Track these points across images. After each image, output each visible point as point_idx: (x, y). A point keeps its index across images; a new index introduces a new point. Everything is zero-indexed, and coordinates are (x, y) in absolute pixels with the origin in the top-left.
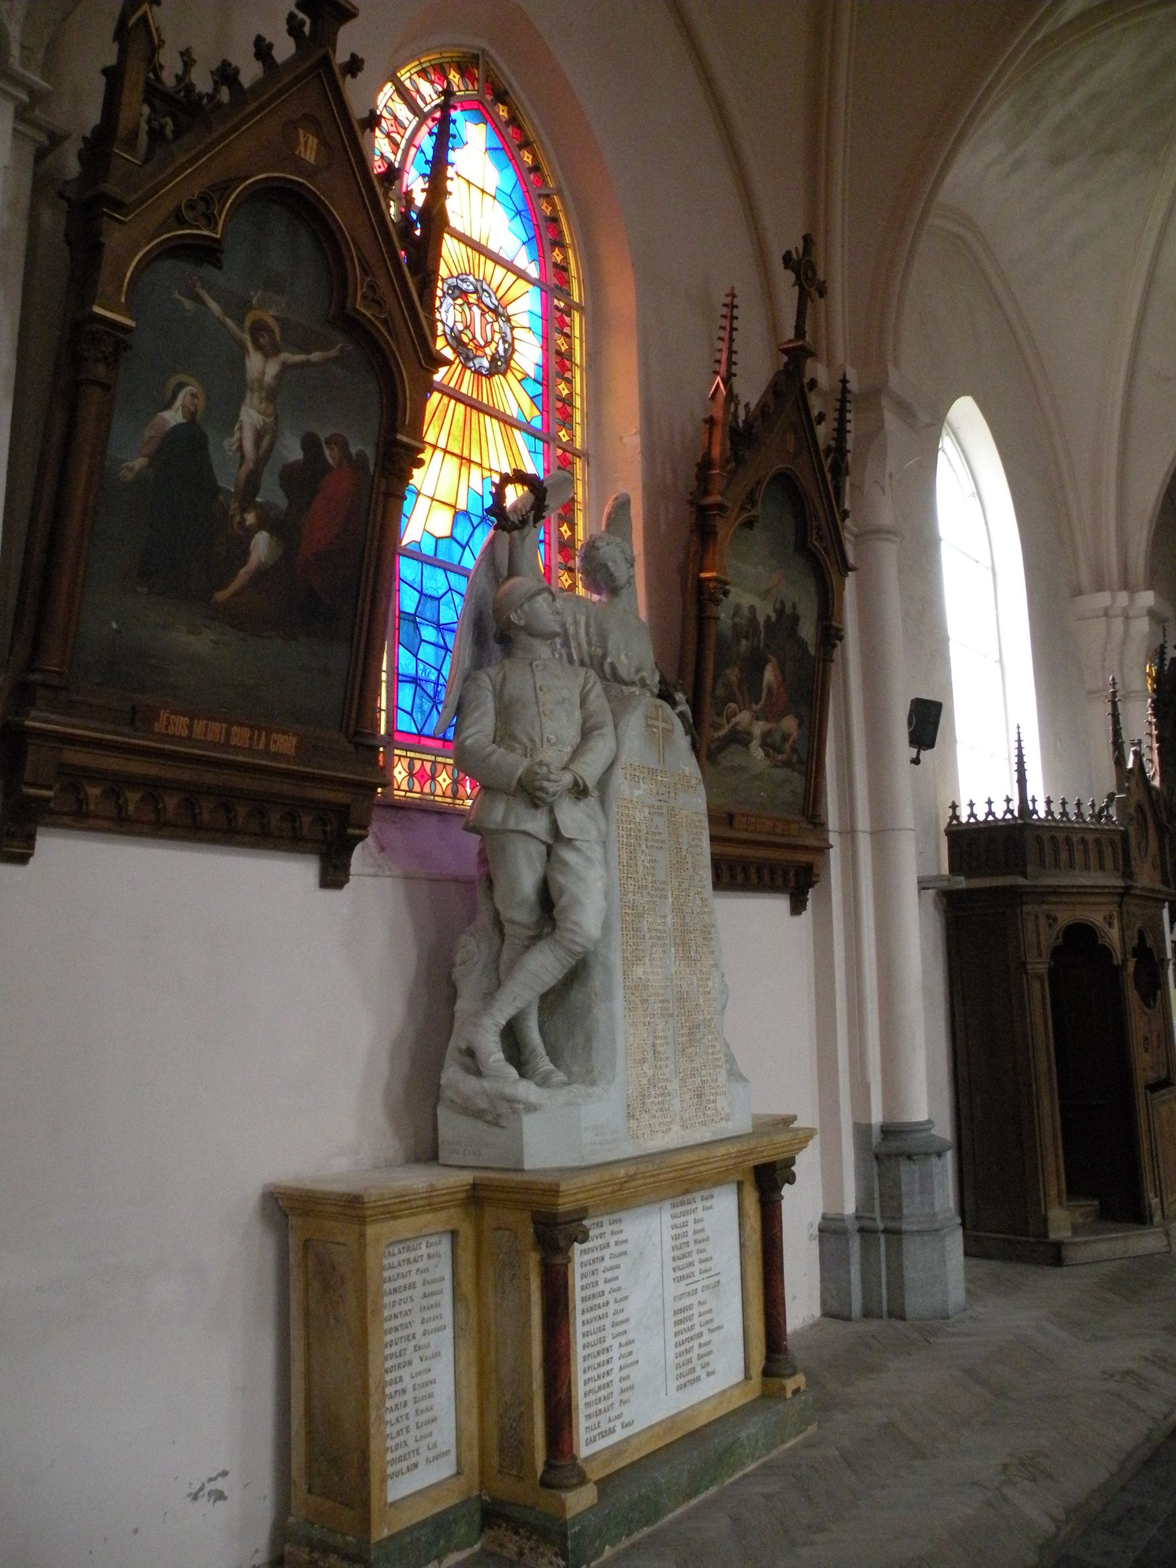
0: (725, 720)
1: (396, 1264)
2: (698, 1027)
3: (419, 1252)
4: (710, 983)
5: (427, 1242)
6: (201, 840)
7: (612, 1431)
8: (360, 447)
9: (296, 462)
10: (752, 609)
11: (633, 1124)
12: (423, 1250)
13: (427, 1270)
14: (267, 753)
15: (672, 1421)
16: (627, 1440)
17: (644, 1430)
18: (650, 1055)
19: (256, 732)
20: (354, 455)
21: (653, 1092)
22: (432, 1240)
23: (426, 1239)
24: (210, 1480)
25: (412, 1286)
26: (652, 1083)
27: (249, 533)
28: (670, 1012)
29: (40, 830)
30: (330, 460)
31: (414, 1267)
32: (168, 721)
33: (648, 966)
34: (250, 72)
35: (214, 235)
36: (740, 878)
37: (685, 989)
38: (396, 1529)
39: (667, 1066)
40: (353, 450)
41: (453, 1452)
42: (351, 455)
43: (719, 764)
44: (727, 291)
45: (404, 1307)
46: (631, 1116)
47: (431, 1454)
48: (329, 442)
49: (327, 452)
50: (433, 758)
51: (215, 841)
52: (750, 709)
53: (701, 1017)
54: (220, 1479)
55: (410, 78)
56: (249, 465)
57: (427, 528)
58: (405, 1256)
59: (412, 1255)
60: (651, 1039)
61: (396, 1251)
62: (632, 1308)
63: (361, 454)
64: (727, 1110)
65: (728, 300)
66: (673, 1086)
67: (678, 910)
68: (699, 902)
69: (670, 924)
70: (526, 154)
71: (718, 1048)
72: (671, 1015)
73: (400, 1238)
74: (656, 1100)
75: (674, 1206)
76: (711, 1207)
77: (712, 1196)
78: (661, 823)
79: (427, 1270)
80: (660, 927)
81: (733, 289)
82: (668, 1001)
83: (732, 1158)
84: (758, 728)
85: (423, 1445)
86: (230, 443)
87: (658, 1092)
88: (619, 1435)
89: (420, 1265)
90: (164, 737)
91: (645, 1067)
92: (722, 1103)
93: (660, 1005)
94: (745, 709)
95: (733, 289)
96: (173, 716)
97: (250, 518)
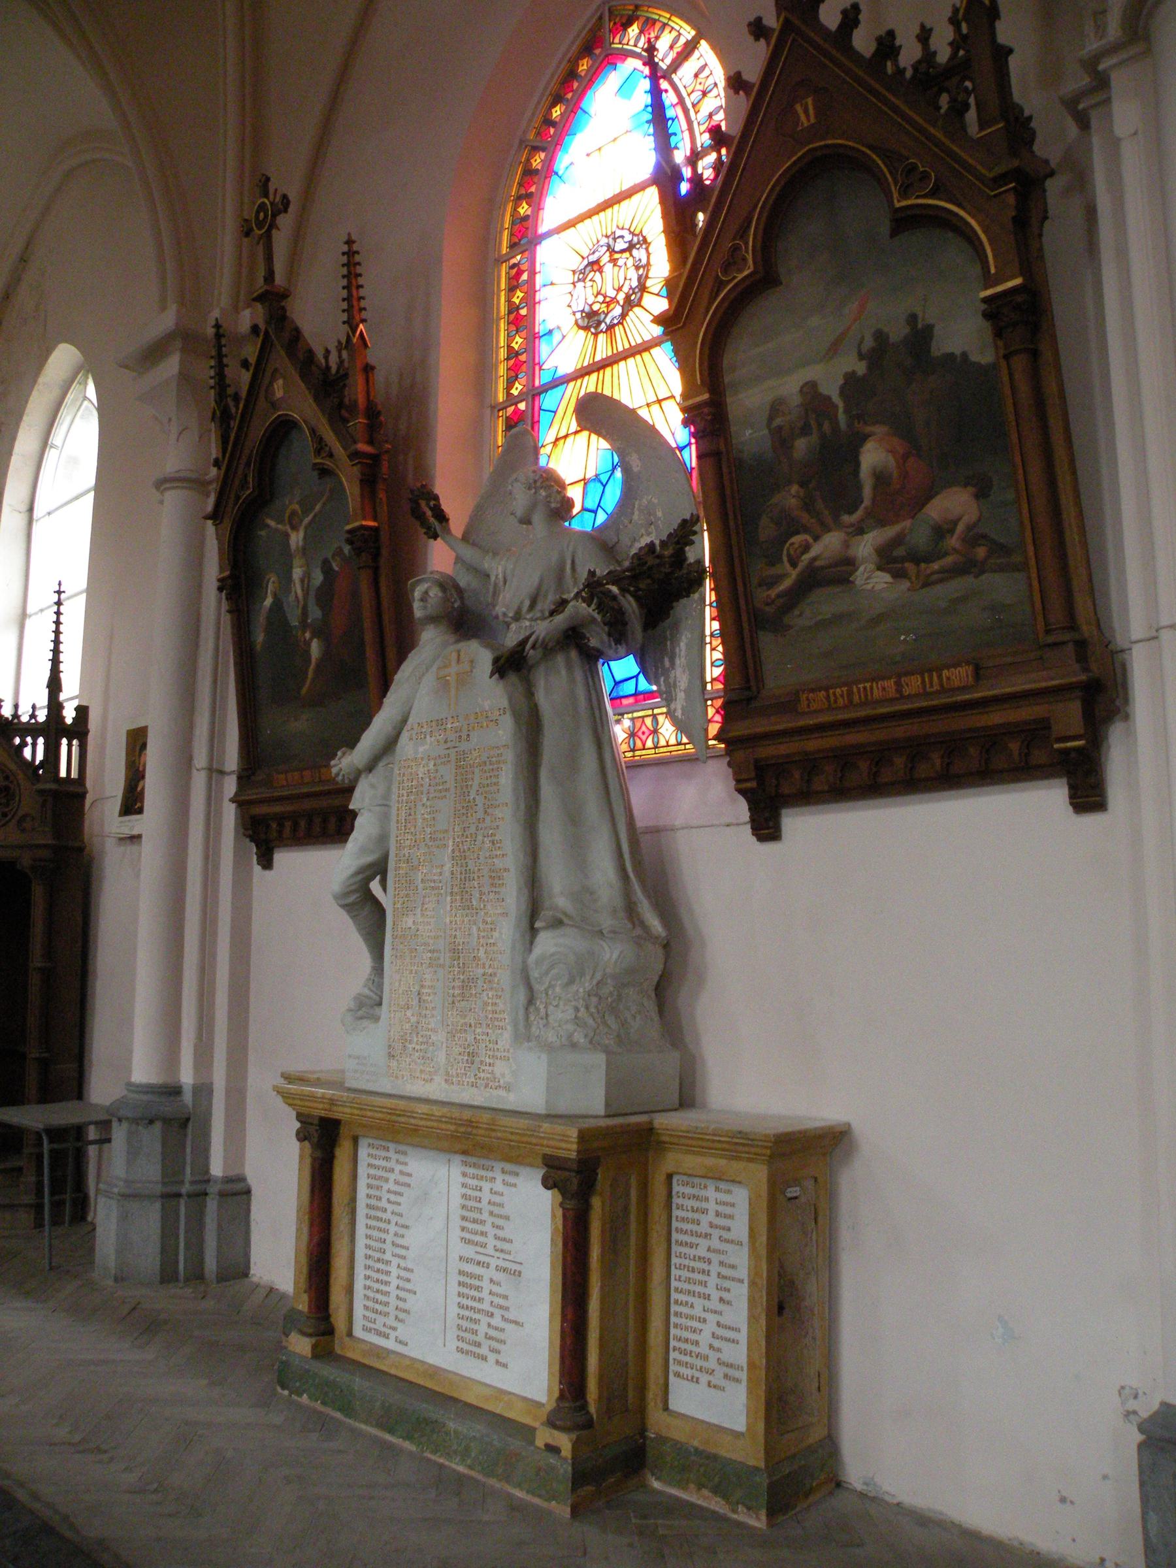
0: (787, 565)
2: (474, 980)
4: (496, 934)
6: (993, 783)
7: (387, 1336)
10: (810, 390)
11: (394, 1064)
14: (943, 690)
15: (435, 1372)
16: (389, 1352)
18: (415, 1002)
19: (926, 675)
21: (415, 1039)
26: (415, 1028)
27: (308, 644)
28: (441, 961)
29: (276, 850)
32: (808, 699)
33: (419, 916)
34: (863, 41)
35: (895, 201)
36: (317, 829)
37: (459, 940)
39: (433, 1016)
43: (790, 627)
44: (345, 238)
46: (391, 1056)
50: (650, 712)
51: (898, 793)
52: (839, 525)
53: (480, 971)
55: (662, 60)
56: (302, 602)
57: (593, 515)
60: (417, 987)
62: (414, 1238)
64: (508, 1078)
65: (345, 248)
66: (440, 1037)
67: (460, 856)
68: (488, 845)
69: (447, 874)
70: (555, 115)
71: (501, 1006)
72: (442, 966)
74: (418, 1047)
75: (465, 1163)
76: (515, 1185)
77: (517, 1174)
78: (448, 773)
80: (436, 878)
81: (349, 234)
82: (438, 951)
83: (324, 1103)
84: (866, 547)
86: (292, 598)
87: (420, 1040)
88: (389, 1344)
91: (409, 1013)
92: (500, 1068)
93: (429, 955)
95: (349, 234)
96: (811, 695)
97: (308, 635)
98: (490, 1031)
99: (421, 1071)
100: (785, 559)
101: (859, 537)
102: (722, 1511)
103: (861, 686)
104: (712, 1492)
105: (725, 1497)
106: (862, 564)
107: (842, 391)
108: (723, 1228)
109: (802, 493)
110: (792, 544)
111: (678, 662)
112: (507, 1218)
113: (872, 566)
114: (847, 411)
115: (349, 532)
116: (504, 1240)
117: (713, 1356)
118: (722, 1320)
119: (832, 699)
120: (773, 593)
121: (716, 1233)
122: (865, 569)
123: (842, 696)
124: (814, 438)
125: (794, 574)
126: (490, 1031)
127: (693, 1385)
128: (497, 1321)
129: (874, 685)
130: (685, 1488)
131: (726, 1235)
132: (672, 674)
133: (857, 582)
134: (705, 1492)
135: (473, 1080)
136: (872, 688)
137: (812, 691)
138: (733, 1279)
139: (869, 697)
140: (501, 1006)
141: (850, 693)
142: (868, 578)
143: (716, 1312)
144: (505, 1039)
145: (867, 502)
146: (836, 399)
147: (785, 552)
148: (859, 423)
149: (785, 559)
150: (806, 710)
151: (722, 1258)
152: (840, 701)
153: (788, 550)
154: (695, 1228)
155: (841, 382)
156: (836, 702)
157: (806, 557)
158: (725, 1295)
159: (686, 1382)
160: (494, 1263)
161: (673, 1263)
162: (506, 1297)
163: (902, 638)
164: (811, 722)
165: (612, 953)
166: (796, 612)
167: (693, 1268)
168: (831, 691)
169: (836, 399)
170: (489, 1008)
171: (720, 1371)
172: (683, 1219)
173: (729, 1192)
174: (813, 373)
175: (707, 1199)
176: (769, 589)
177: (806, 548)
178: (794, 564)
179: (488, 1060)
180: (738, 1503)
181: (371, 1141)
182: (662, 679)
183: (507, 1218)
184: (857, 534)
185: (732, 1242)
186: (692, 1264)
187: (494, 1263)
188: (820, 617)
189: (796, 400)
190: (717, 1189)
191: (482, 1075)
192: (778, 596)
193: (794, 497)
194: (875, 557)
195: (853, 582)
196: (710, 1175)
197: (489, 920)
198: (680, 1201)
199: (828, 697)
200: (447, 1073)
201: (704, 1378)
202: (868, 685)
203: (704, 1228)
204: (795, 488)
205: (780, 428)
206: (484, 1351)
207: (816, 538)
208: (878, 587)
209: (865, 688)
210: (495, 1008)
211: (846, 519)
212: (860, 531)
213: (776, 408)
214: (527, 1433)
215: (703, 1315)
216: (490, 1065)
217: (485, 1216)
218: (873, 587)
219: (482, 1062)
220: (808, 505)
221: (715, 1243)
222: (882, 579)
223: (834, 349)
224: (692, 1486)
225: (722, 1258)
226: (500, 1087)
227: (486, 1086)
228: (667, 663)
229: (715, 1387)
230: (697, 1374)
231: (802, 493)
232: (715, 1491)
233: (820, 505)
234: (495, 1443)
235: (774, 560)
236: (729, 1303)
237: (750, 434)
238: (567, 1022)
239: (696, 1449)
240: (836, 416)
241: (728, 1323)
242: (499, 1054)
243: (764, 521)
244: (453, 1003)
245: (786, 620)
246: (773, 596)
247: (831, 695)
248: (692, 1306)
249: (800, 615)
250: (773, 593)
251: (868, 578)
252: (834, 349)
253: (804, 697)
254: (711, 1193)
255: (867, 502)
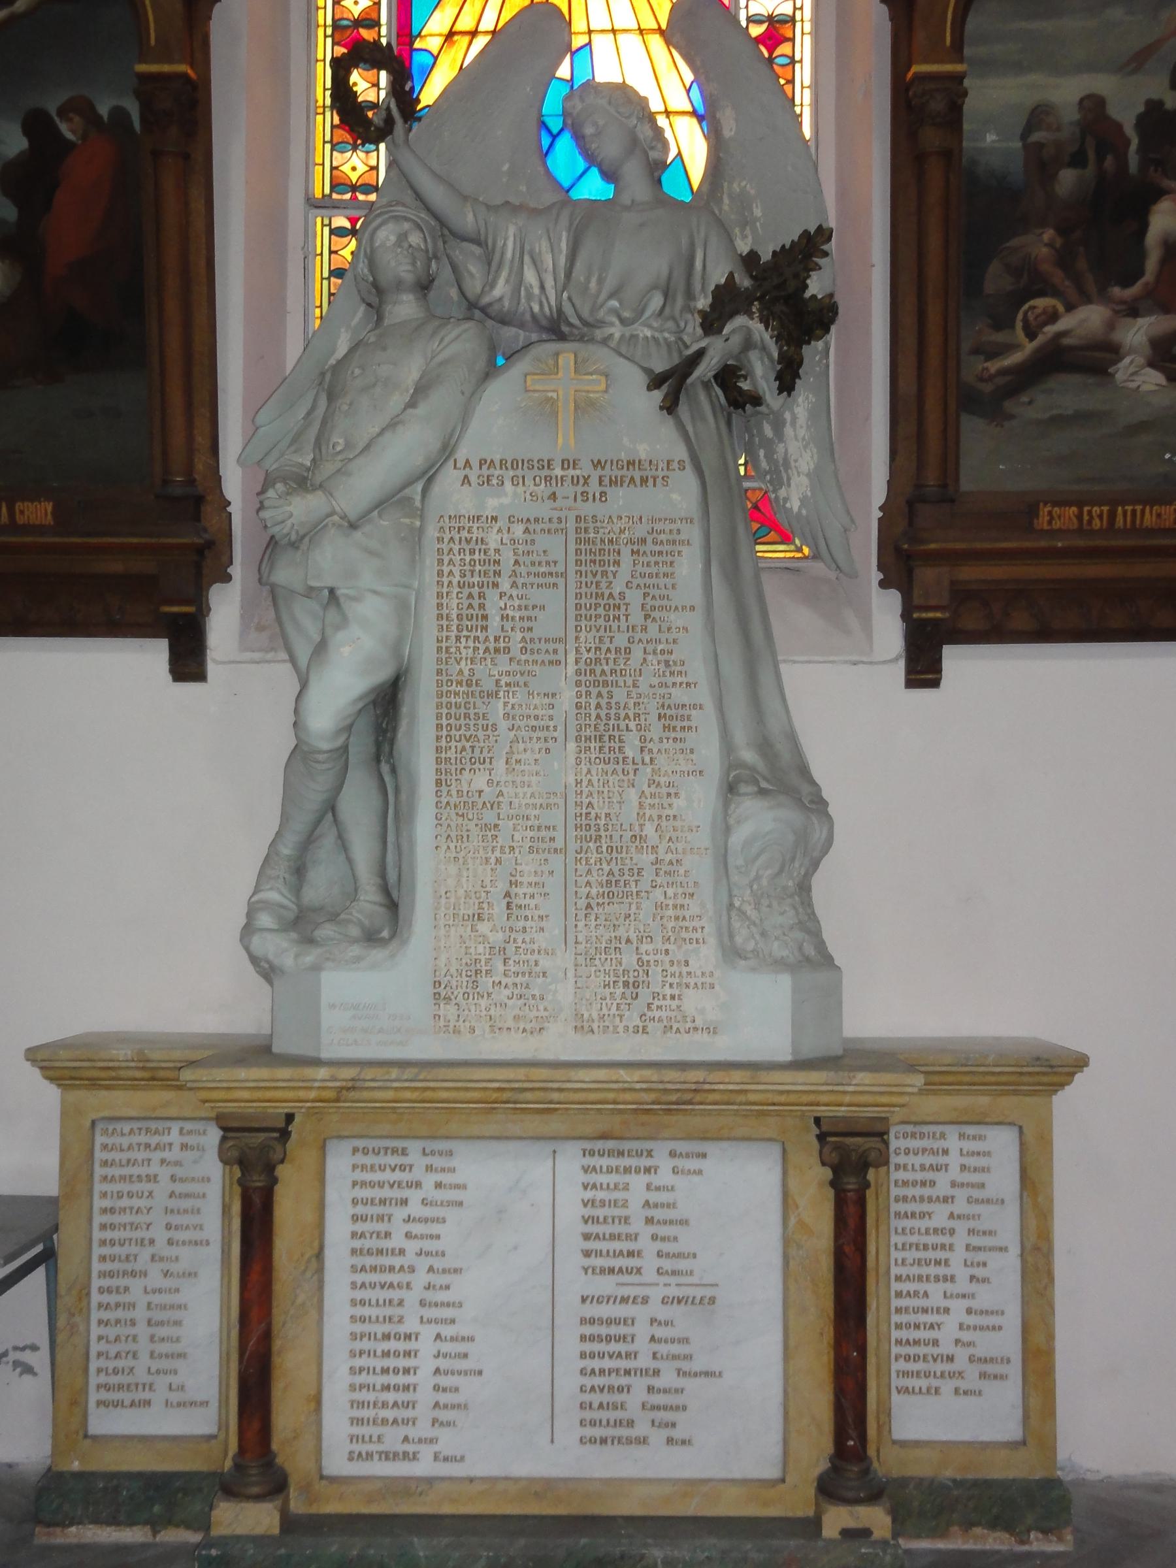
1: (125, 1146)
3: (166, 1139)
4: (679, 803)
5: (181, 1129)
8: (114, 102)
9: (22, 153)
10: (1094, 105)
12: (174, 1137)
13: (178, 1163)
15: (545, 1487)
16: (430, 1481)
17: (165, 1438)
18: (499, 908)
20: (105, 117)
22: (188, 1126)
23: (181, 1124)
24: (16, 1348)
25: (153, 1178)
30: (70, 136)
31: (157, 1156)
32: (1050, 513)
37: (600, 808)
38: (92, 1467)
40: (103, 110)
41: (214, 1404)
42: (101, 117)
45: (136, 1203)
47: (175, 1397)
48: (62, 112)
49: (64, 128)
52: (1103, 296)
54: (28, 1352)
58: (143, 1139)
59: (154, 1140)
61: (126, 1130)
63: (119, 114)
71: (694, 909)
73: (118, 1114)
77: (450, 1153)
79: (178, 1163)
85: (162, 1382)
88: (424, 1467)
89: (166, 1155)
90: (1052, 533)
94: (1088, 301)
96: (1056, 509)
98: (671, 947)
99: (516, 1018)
100: (1019, 325)
101: (1129, 320)
102: (1004, 1548)
103: (1129, 508)
104: (61, 1475)
105: (1009, 1528)
106: (1128, 354)
107: (1142, 122)
108: (972, 1185)
109: (1059, 242)
110: (1033, 308)
111: (788, 431)
112: (684, 1222)
113: (1140, 360)
114: (1141, 149)
115: (144, 78)
116: (679, 1255)
117: (962, 1354)
118: (974, 1304)
119: (1086, 518)
120: (994, 366)
121: (961, 1194)
122: (1132, 362)
123: (1100, 516)
124: (1090, 171)
125: (1030, 347)
126: (671, 947)
127: (932, 1399)
128: (668, 1378)
129: (1148, 508)
130: (943, 1534)
131: (976, 1193)
132: (780, 448)
133: (1117, 376)
134: (978, 1530)
135: (638, 1022)
136: (1143, 512)
137: (1056, 504)
138: (991, 1249)
139: (1138, 522)
140: (694, 909)
141: (1112, 515)
142: (1135, 373)
143: (964, 1296)
144: (706, 956)
145: (1150, 274)
146: (1129, 130)
147: (1020, 316)
148: (1156, 171)
149: (1019, 325)
150: (1046, 527)
151: (972, 1224)
152: (1097, 524)
153: (1026, 313)
154: (927, 1192)
155: (1141, 109)
156: (1090, 522)
157: (1051, 330)
158: (979, 1272)
159: (920, 1397)
160: (656, 1294)
161: (892, 1243)
162: (685, 1341)
163: (1167, 456)
164: (1060, 545)
165: (821, 831)
166: (1025, 399)
167: (917, 1249)
168: (1086, 509)
169: (1129, 130)
170: (670, 912)
171: (973, 1371)
172: (905, 1183)
173: (981, 1138)
174: (1102, 84)
175: (946, 1152)
176: (986, 360)
177: (1053, 317)
178: (1031, 336)
179: (668, 991)
180: (1029, 1531)
181: (672, 1145)
182: (762, 453)
183: (684, 1222)
184: (1128, 315)
185: (988, 1201)
186: (925, 1239)
187: (656, 1294)
188: (1055, 412)
189: (1070, 115)
190: (962, 1136)
191: (657, 1014)
192: (1003, 372)
193: (1046, 245)
194: (1147, 350)
195: (1112, 375)
196: (965, 1119)
197: (663, 780)
198: (902, 1159)
199: (1080, 517)
200: (579, 1016)
201: (947, 1386)
202: (1139, 508)
203: (943, 1189)
204: (1048, 234)
205: (1040, 146)
206: (641, 1429)
207: (1070, 308)
208: (1146, 388)
209: (1134, 512)
210: (680, 913)
211: (1116, 291)
212: (1133, 311)
213: (1038, 116)
214: (811, 1526)
215: (944, 1303)
216: (673, 997)
217: (637, 1225)
218: (1139, 387)
219: (655, 995)
220: (1064, 260)
221: (960, 1207)
222: (1152, 379)
223: (1137, 62)
224: (955, 1529)
225: (972, 1224)
226: (696, 1029)
227: (668, 1029)
228: (768, 431)
229: (965, 1393)
230: (935, 1383)
231: (1059, 242)
232: (993, 1525)
233: (1082, 264)
234: (753, 1555)
235: (1003, 322)
236: (985, 1280)
237: (993, 142)
238: (791, 928)
239: (954, 1481)
240: (1126, 154)
241: (985, 1306)
242: (692, 981)
243: (995, 268)
244: (589, 906)
245: (1009, 405)
246: (993, 370)
247: (1085, 513)
248: (926, 1294)
249: (1030, 403)
250: (994, 366)
251: (1135, 373)
252: (1137, 62)
253: (1044, 510)
254: (953, 1142)
255: (1150, 274)
